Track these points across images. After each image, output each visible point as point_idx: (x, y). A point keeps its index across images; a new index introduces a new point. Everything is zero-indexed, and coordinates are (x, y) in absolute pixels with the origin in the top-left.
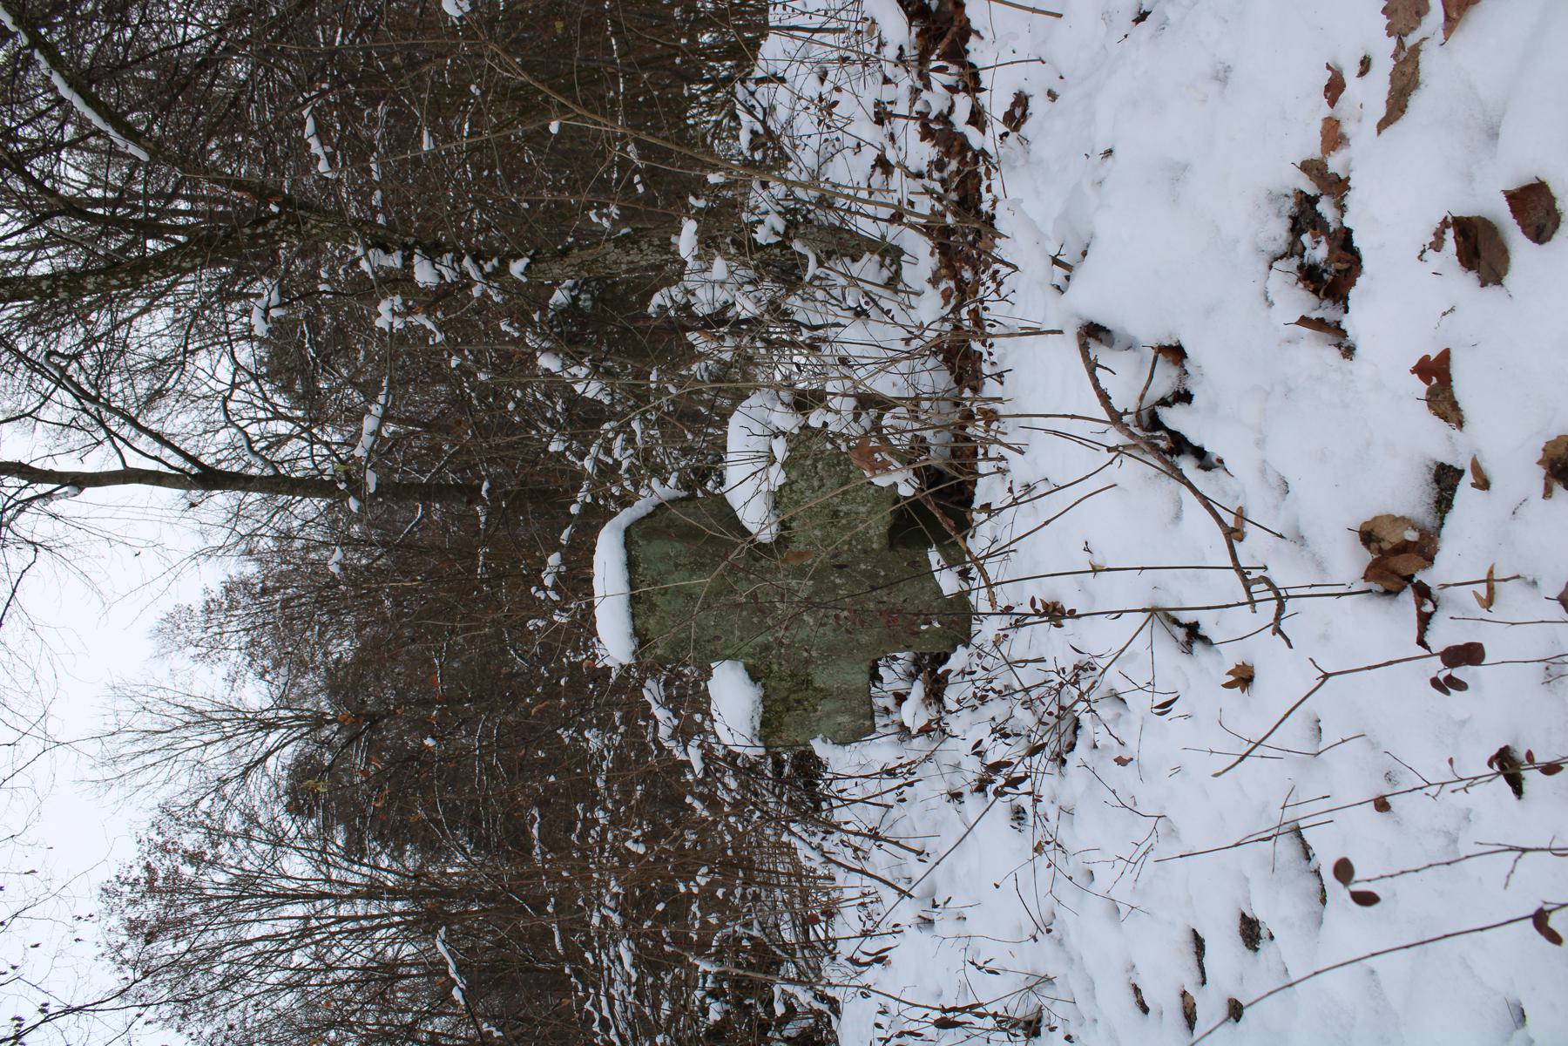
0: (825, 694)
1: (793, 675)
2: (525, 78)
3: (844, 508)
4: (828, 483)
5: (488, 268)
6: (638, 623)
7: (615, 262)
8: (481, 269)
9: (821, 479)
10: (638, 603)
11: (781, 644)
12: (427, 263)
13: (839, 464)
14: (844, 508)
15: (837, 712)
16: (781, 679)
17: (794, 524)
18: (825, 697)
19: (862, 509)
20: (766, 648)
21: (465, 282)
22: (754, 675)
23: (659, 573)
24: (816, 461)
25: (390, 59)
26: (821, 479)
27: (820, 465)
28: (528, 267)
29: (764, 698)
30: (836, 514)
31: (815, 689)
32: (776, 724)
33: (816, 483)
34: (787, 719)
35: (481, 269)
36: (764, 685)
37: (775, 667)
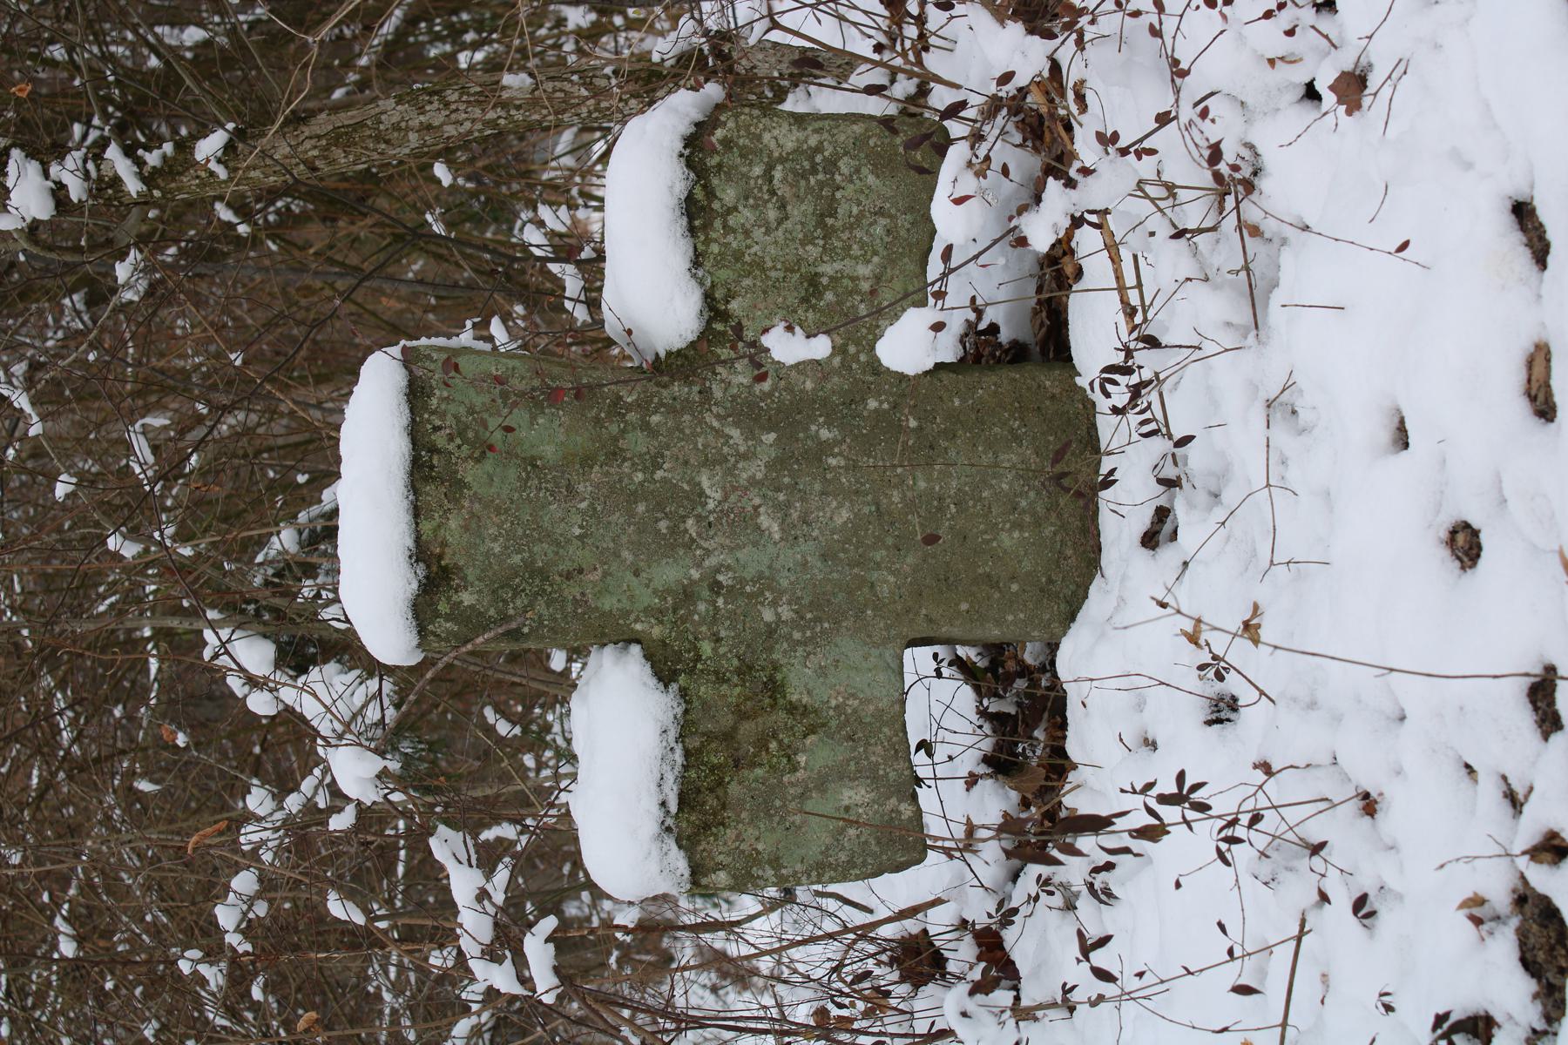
0: (809, 719)
1: (746, 670)
2: (387, 1011)
3: (828, 269)
4: (795, 211)
5: (153, 159)
6: (426, 527)
7: (396, 127)
8: (140, 163)
9: (782, 206)
10: (426, 471)
11: (716, 587)
12: (33, 168)
13: (814, 171)
14: (828, 269)
15: (841, 775)
16: (721, 679)
17: (734, 305)
18: (812, 730)
19: (863, 270)
20: (687, 595)
21: (174, 538)
22: (664, 670)
23: (471, 411)
24: (770, 168)
25: (143, 919)
26: (782, 206)
27: (778, 174)
28: (229, 147)
29: (686, 727)
30: (813, 281)
31: (792, 709)
32: (711, 802)
33: (772, 214)
34: (734, 789)
35: (140, 163)
36: (684, 693)
37: (706, 648)
